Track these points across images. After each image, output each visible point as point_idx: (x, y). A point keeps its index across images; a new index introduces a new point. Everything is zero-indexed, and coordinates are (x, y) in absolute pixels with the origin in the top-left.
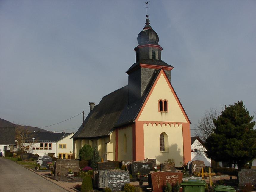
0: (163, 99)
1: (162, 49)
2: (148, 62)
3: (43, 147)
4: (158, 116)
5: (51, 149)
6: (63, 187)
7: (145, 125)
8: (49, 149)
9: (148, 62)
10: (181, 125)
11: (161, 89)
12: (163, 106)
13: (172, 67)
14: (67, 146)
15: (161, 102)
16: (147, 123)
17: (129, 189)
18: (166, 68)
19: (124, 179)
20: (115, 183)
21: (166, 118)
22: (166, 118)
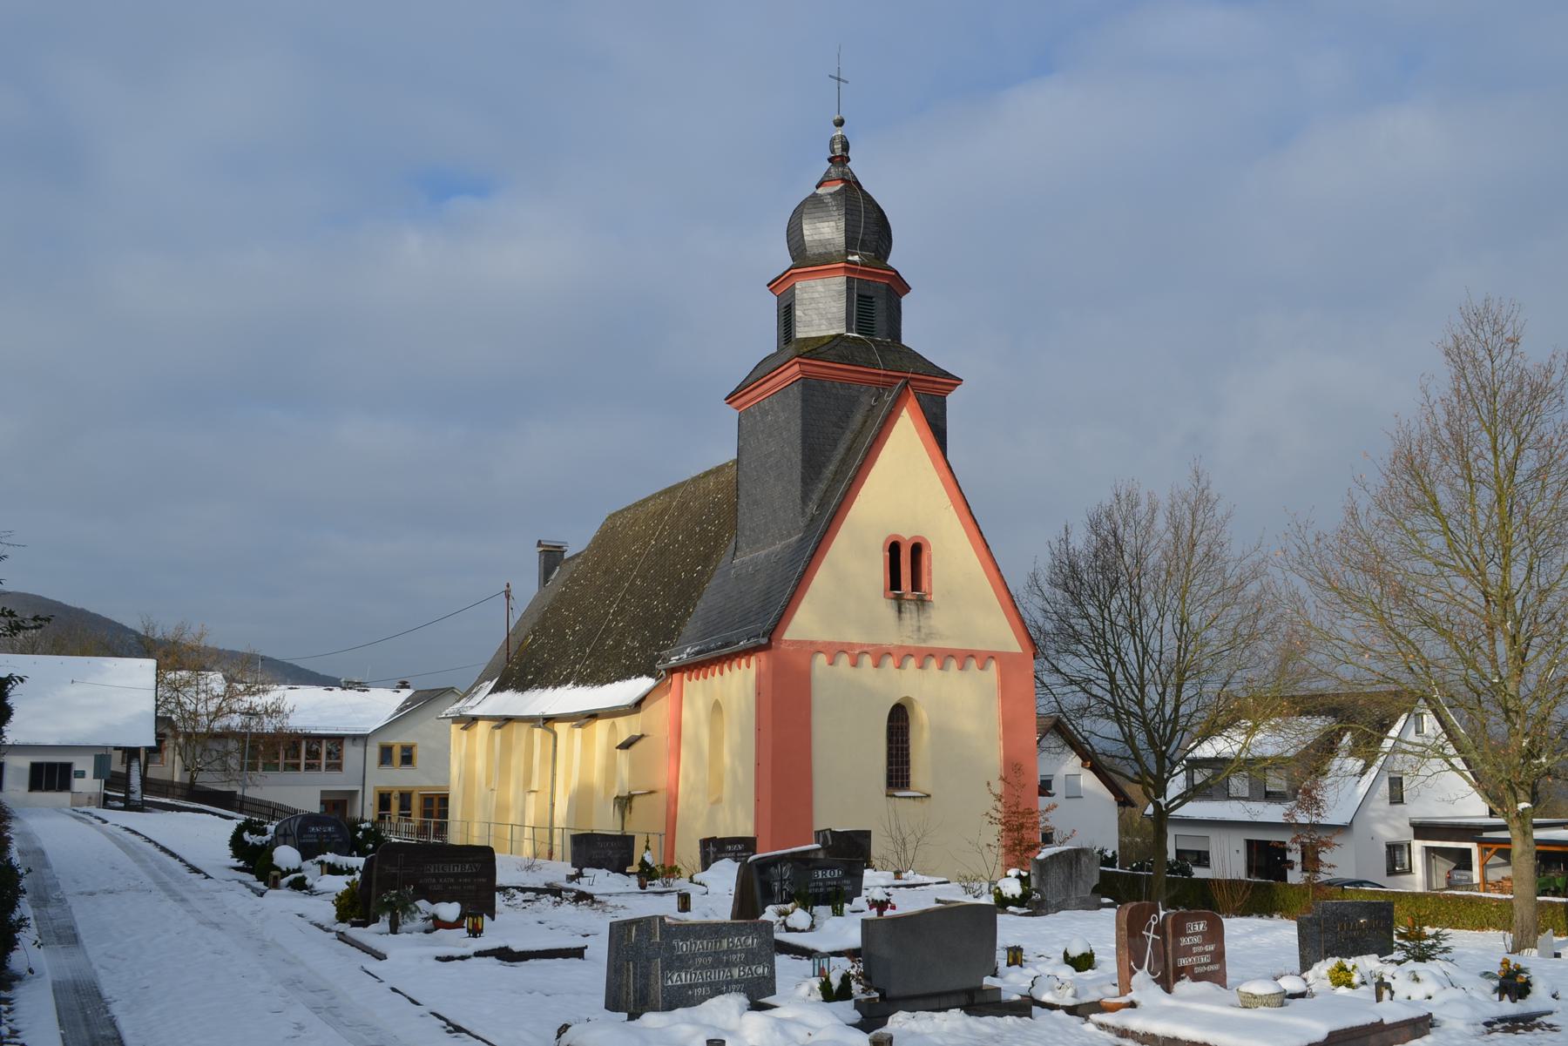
0: (907, 534)
1: (907, 289)
2: (857, 375)
3: (298, 757)
4: (888, 627)
5: (338, 767)
6: (170, 902)
7: (821, 660)
8: (328, 766)
9: (857, 375)
10: (993, 665)
11: (900, 483)
12: (905, 565)
13: (946, 374)
14: (418, 754)
15: (894, 549)
16: (834, 651)
17: (228, 753)
18: (931, 392)
19: (746, 962)
20: (696, 986)
21: (919, 629)
22: (919, 629)
